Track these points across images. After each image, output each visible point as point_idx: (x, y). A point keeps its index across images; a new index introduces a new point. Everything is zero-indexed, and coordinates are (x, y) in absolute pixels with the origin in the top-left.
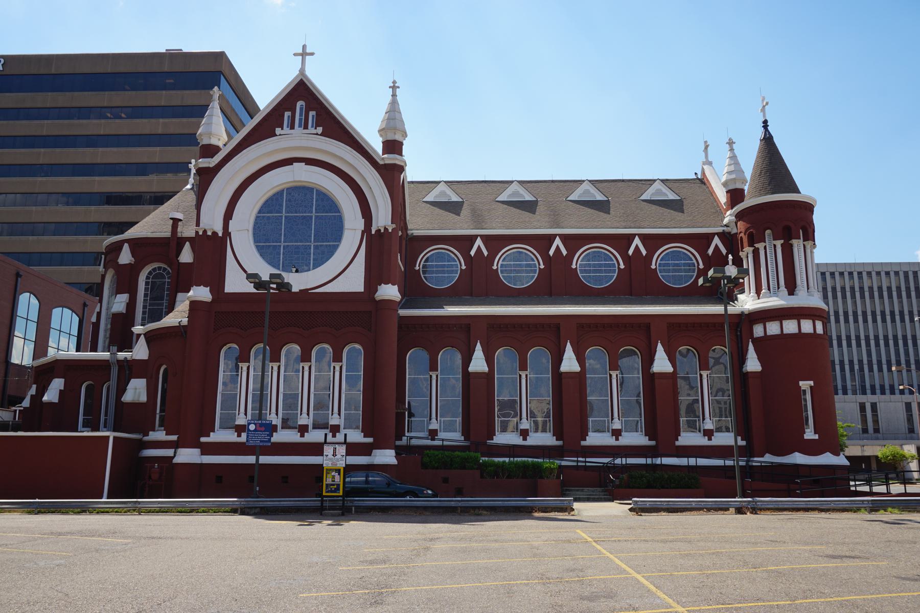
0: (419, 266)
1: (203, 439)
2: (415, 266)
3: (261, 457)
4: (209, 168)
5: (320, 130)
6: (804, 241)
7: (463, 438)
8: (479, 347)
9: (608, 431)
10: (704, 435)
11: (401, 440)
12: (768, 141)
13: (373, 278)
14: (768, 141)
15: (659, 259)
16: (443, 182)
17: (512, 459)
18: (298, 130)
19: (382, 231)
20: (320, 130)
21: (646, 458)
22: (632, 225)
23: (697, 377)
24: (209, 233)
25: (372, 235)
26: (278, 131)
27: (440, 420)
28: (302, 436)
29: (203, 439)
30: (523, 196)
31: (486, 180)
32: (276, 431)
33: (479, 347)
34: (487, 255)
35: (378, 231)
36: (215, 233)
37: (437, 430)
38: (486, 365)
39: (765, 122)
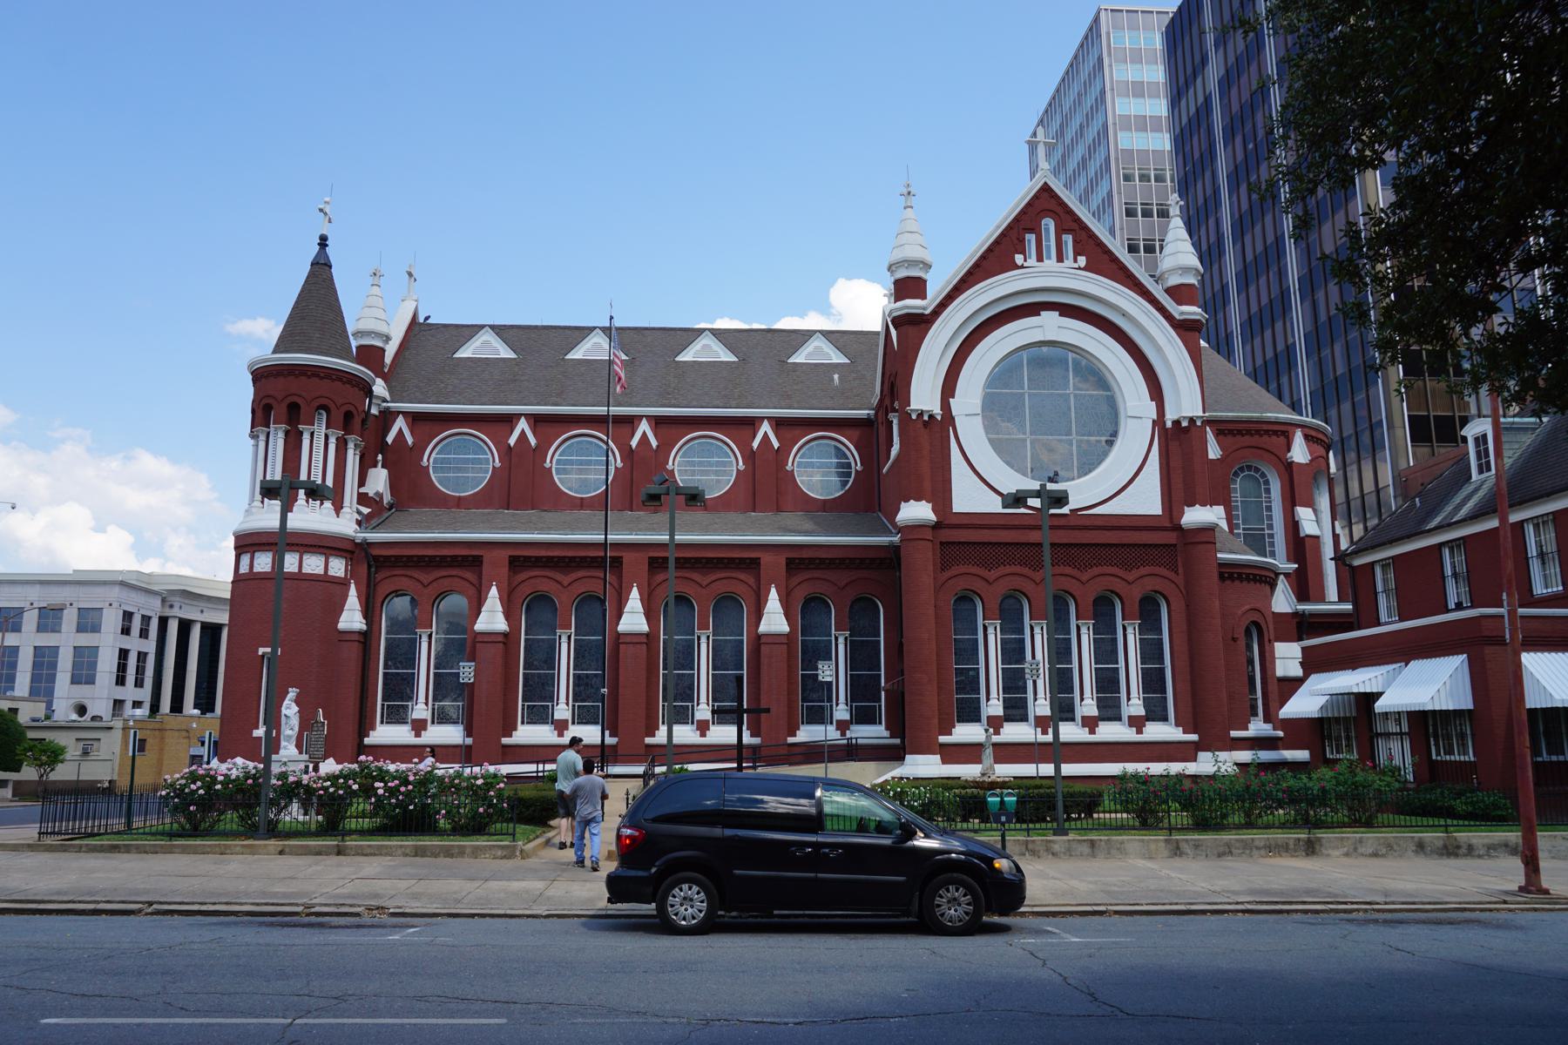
0: (551, 462)
1: (943, 739)
2: (545, 462)
3: (1063, 766)
4: (923, 315)
5: (1082, 261)
6: (327, 428)
7: (886, 734)
8: (773, 594)
9: (693, 723)
10: (1083, 726)
11: (1247, 729)
12: (321, 267)
13: (1177, 490)
14: (321, 267)
15: (558, 453)
16: (707, 332)
17: (541, 767)
18: (1050, 263)
19: (1185, 424)
20: (1082, 261)
21: (538, 763)
22: (704, 404)
23: (831, 641)
24: (1185, 424)
25: (1167, 429)
26: (1019, 259)
27: (574, 706)
28: (418, 735)
29: (943, 739)
30: (497, 351)
31: (652, 326)
32: (425, 729)
33: (773, 594)
34: (658, 446)
35: (1177, 423)
36: (931, 417)
37: (567, 721)
38: (645, 622)
39: (323, 242)
